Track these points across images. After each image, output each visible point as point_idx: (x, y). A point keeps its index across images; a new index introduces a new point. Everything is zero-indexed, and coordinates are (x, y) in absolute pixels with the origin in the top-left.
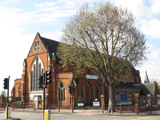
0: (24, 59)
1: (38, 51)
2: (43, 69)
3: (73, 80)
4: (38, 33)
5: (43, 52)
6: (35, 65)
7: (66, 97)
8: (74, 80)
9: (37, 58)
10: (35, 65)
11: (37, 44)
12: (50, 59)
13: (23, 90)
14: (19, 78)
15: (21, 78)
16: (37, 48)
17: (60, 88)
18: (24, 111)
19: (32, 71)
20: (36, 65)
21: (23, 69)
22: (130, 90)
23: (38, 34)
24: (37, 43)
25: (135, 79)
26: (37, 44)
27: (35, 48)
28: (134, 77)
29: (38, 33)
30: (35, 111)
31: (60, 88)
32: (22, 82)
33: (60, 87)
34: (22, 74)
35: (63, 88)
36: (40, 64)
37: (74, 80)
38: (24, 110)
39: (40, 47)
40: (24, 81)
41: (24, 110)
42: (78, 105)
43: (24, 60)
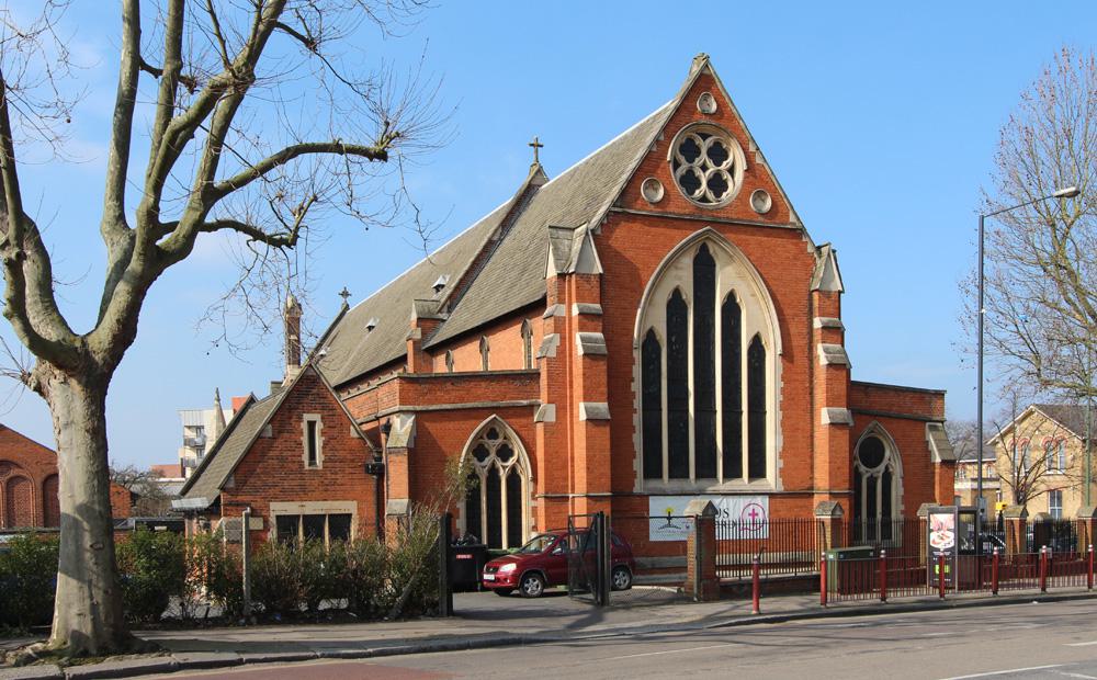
5: (760, 221)
6: (677, 292)
10: (677, 292)
17: (863, 468)
20: (688, 294)
26: (705, 145)
36: (731, 297)
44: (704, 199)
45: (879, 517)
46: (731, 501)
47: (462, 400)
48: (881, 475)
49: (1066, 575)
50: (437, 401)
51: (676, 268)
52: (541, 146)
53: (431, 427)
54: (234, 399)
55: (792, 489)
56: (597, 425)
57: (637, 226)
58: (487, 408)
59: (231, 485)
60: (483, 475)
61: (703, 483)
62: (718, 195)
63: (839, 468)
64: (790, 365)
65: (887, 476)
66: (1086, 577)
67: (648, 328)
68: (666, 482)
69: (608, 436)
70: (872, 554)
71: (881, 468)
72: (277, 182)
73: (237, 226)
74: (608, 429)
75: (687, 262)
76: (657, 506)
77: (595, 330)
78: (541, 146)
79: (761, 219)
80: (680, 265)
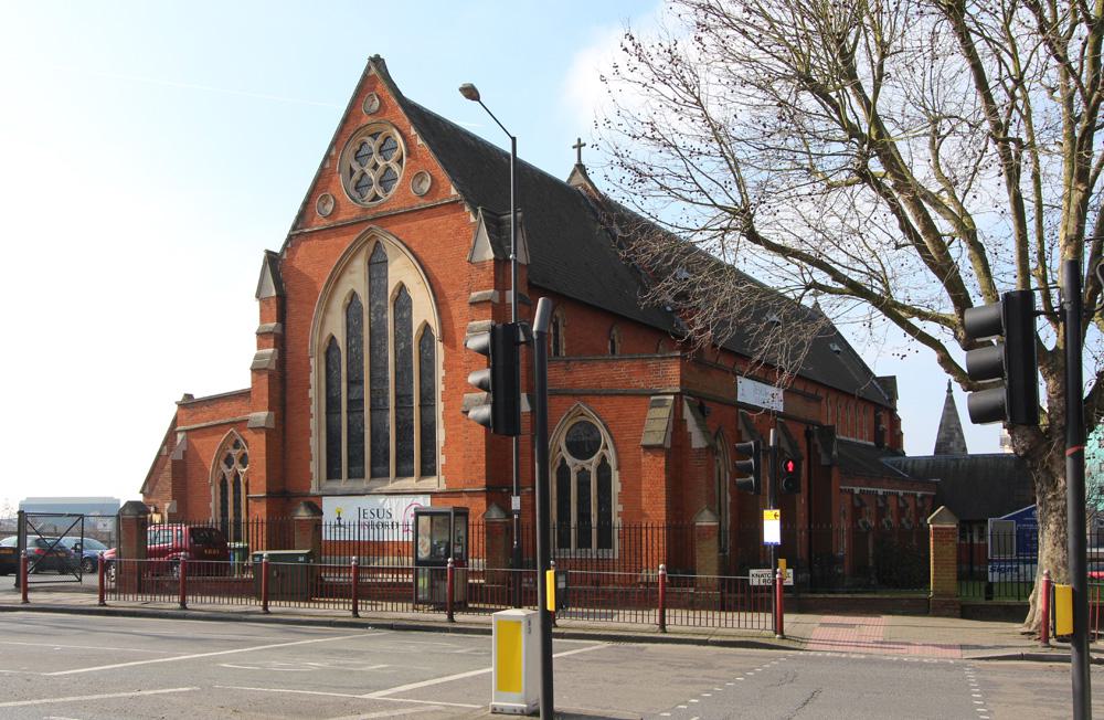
0: (263, 254)
1: (376, 198)
2: (426, 327)
3: (682, 405)
4: (378, 57)
5: (424, 203)
6: (353, 295)
7: (616, 521)
8: (686, 403)
9: (373, 243)
10: (353, 295)
11: (373, 145)
12: (494, 252)
13: (486, 454)
14: (197, 396)
15: (243, 381)
16: (372, 175)
17: (570, 460)
18: (183, 614)
19: (332, 339)
20: (364, 300)
21: (255, 324)
22: (901, 493)
23: (376, 74)
24: (374, 136)
25: (876, 428)
26: (373, 145)
27: (356, 176)
28: (872, 418)
29: (378, 57)
30: (268, 613)
31: (570, 460)
32: (261, 416)
33: (565, 453)
34: (249, 362)
35: (592, 464)
36: (402, 287)
37: (686, 403)
38: (265, 607)
39: (396, 168)
40: (270, 409)
41: (265, 607)
42: (548, 572)
43: (258, 261)
44: (376, 198)
45: (594, 521)
46: (394, 500)
47: (213, 419)
48: (579, 461)
49: (755, 611)
50: (198, 421)
51: (351, 273)
52: (579, 140)
53: (197, 442)
54: (894, 377)
55: (454, 488)
56: (256, 433)
57: (315, 242)
58: (226, 424)
59: (147, 491)
60: (230, 480)
61: (376, 482)
62: (386, 191)
63: (474, 463)
64: (450, 350)
65: (604, 468)
66: (658, 612)
67: (326, 335)
68: (343, 484)
69: (264, 442)
70: (301, 559)
71: (595, 459)
72: (750, 176)
73: (965, 194)
74: (264, 436)
75: (360, 264)
76: (330, 507)
77: (268, 347)
78: (579, 140)
79: (422, 201)
80: (352, 270)
